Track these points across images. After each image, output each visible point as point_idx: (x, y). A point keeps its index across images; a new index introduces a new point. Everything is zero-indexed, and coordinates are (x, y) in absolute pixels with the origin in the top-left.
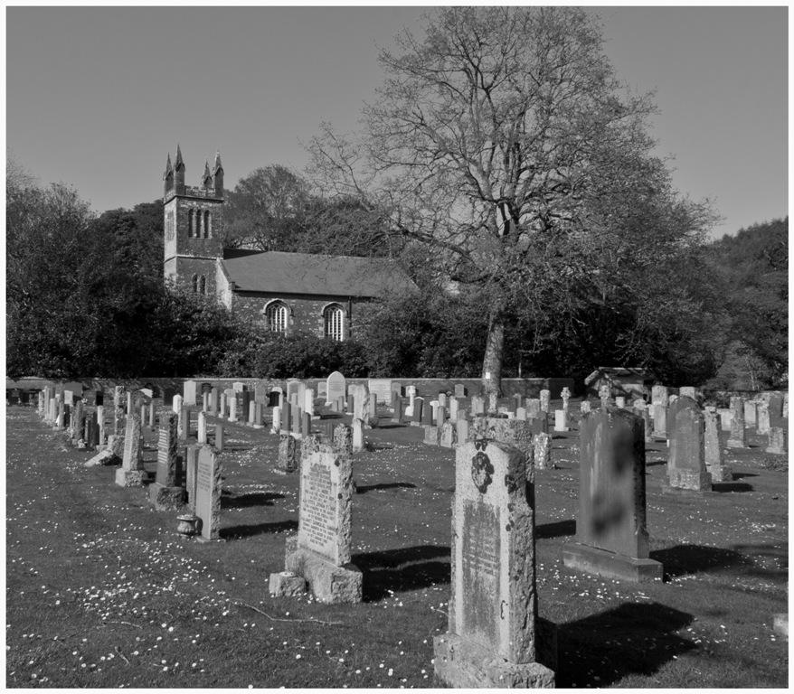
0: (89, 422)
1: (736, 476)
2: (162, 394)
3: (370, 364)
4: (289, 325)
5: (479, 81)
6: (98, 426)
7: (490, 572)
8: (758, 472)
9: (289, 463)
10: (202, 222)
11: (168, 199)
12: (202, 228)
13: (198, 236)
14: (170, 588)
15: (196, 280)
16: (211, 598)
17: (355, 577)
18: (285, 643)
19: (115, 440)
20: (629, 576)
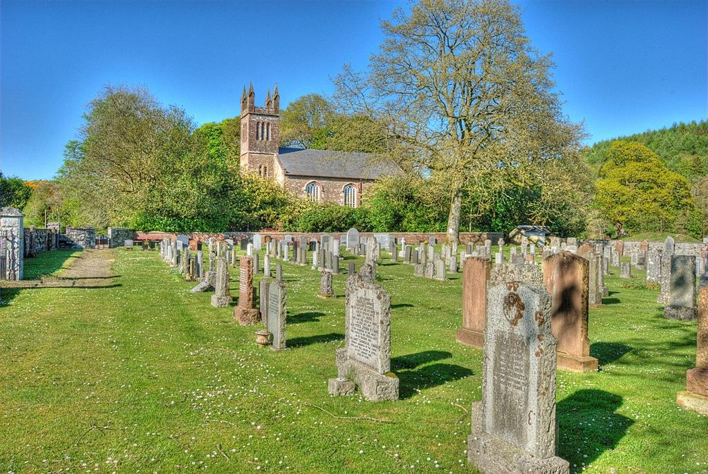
0: (193, 262)
1: (610, 293)
2: (239, 243)
3: (374, 223)
4: (321, 197)
5: (446, 42)
6: (198, 265)
7: (520, 388)
8: (619, 290)
9: (328, 291)
10: (265, 130)
11: (244, 115)
12: (265, 134)
13: (262, 139)
14: (255, 391)
15: (261, 167)
16: (286, 399)
17: (394, 381)
18: (349, 439)
19: (210, 274)
20: (577, 369)
